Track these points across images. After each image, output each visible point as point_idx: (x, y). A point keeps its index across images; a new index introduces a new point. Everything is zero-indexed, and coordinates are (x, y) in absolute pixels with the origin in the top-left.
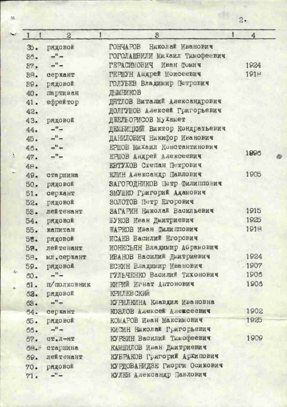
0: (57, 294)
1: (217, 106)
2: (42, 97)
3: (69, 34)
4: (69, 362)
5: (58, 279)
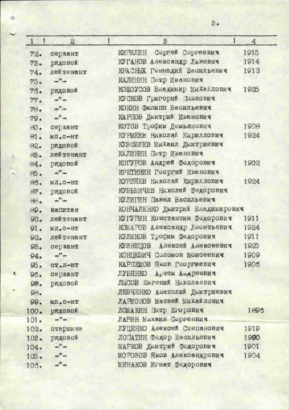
0: (61, 165)
1: (218, 140)
2: (46, 160)
3: (73, 40)
4: (72, 160)
5: (61, 178)
